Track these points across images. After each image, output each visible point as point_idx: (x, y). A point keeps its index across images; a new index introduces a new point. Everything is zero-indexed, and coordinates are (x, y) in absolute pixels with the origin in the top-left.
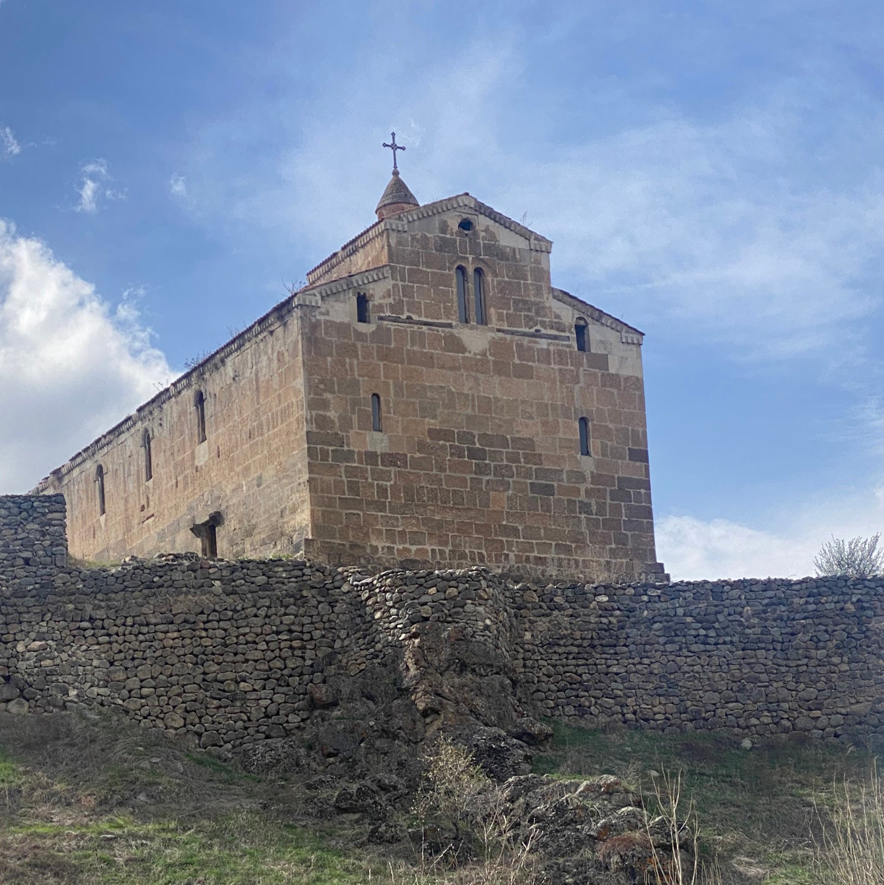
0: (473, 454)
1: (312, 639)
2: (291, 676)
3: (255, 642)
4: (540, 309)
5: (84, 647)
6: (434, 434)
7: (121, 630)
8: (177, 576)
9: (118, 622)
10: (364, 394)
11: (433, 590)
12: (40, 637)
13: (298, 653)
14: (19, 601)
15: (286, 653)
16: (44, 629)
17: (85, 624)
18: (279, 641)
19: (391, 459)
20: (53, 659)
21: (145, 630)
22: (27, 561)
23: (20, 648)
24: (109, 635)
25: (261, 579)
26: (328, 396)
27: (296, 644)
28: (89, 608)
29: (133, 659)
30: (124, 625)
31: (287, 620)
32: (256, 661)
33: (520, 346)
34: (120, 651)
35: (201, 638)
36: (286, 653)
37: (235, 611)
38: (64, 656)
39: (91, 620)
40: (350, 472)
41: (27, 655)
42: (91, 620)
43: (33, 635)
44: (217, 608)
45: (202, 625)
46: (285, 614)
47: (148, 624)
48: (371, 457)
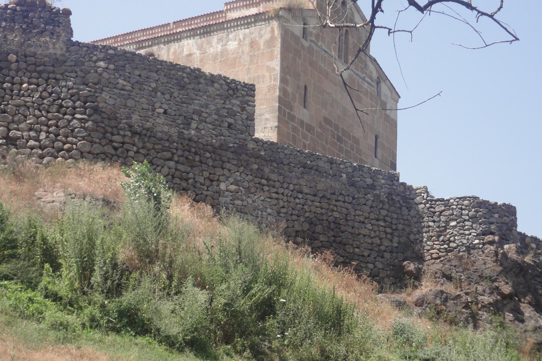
0: (339, 139)
1: (396, 229)
2: (385, 251)
3: (363, 222)
4: (366, 65)
5: (262, 198)
6: (327, 121)
7: (286, 191)
8: (321, 164)
9: (285, 185)
10: (302, 85)
11: (496, 216)
12: (236, 183)
13: (389, 236)
14: (224, 153)
15: (383, 235)
16: (239, 178)
17: (264, 181)
18: (378, 226)
19: (310, 128)
20: (242, 201)
21: (300, 196)
22: (230, 126)
23: (223, 186)
24: (277, 193)
25: (369, 181)
26: (288, 77)
27: (389, 230)
28: (267, 170)
29: (291, 215)
30: (287, 188)
31: (384, 213)
32: (364, 236)
33: (358, 83)
34: (283, 207)
35: (333, 211)
36: (383, 235)
37: (354, 198)
38: (250, 201)
39: (268, 179)
40: (294, 129)
41: (226, 193)
42: (268, 179)
43: (231, 180)
44: (343, 192)
45: (334, 202)
46: (382, 209)
47: (301, 192)
48: (302, 123)
